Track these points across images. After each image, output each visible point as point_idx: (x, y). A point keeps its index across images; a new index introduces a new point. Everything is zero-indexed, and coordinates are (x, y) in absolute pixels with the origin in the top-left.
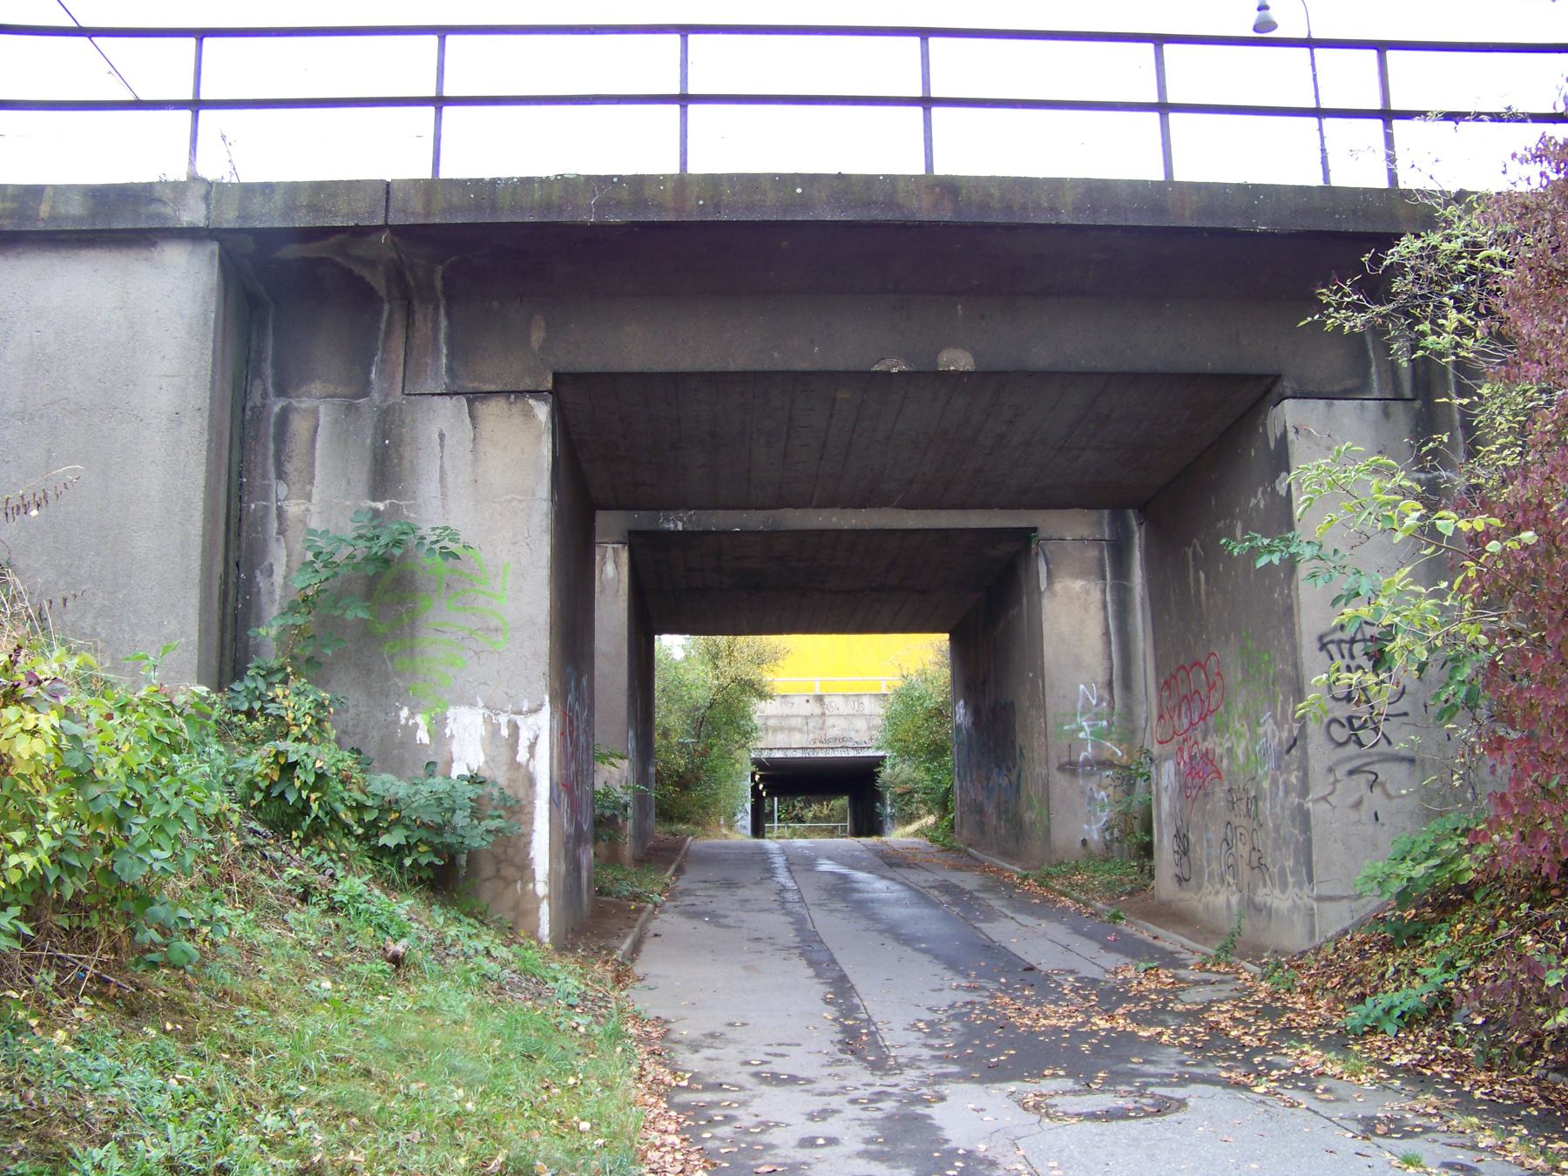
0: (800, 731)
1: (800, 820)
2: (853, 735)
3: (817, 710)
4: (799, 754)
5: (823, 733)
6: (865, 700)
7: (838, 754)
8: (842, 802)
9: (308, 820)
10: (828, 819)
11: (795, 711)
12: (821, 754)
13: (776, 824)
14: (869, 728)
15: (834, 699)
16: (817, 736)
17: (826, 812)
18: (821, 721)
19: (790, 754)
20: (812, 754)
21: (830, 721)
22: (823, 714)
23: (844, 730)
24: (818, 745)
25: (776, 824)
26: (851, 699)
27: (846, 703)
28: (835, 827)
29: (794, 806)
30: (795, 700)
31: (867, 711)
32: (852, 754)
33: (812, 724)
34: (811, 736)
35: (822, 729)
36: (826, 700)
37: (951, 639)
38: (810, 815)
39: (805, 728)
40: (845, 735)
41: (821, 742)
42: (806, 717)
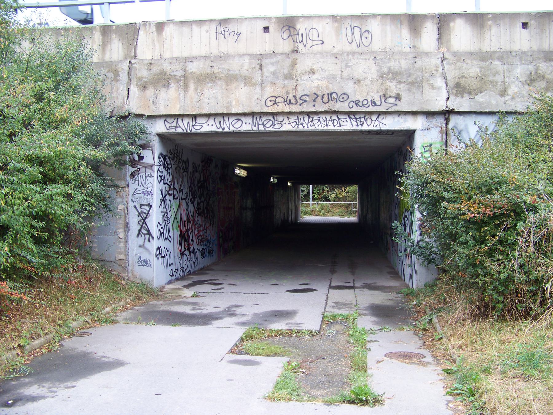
0: (248, 81)
1: (327, 199)
2: (349, 88)
3: (285, 46)
4: (246, 126)
5: (290, 84)
6: (374, 26)
7: (318, 125)
8: (354, 188)
9: (400, 173)
10: (345, 199)
11: (241, 48)
12: (288, 126)
13: (311, 202)
14: (382, 76)
15: (315, 24)
16: (280, 91)
17: (343, 194)
18: (288, 62)
19: (230, 126)
20: (269, 125)
21: (304, 64)
22: (296, 51)
23: (332, 78)
24: (282, 107)
25: (311, 202)
26: (347, 23)
27: (338, 31)
28: (349, 204)
29: (323, 190)
30: (243, 28)
31: (376, 46)
32: (348, 125)
33: (269, 69)
34: (269, 91)
35: (289, 76)
36: (301, 27)
37: (359, 188)
38: (333, 196)
39: (257, 77)
40: (333, 88)
41: (287, 102)
42: (261, 57)
